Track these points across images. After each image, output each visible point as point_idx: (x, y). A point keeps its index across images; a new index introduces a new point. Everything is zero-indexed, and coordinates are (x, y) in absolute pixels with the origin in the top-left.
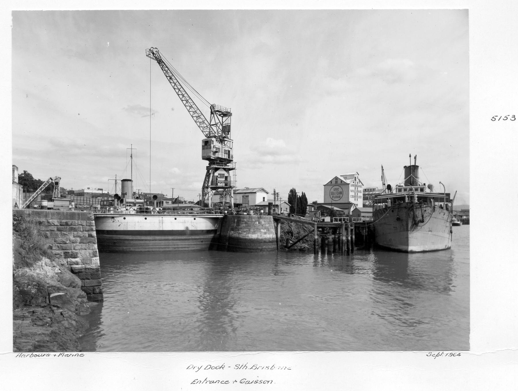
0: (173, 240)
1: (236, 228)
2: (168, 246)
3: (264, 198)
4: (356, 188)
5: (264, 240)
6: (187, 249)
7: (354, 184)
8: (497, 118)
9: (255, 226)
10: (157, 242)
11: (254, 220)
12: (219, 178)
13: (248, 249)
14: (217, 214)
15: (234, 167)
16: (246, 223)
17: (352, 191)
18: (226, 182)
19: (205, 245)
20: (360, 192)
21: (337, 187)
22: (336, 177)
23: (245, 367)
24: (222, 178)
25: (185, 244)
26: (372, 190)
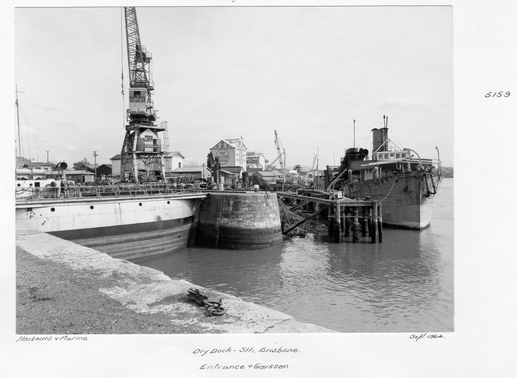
0: (139, 240)
1: (233, 213)
2: (133, 252)
3: (180, 163)
4: (241, 152)
5: (274, 229)
6: (161, 252)
7: (239, 148)
8: (492, 95)
9: (262, 210)
10: (114, 246)
11: (260, 201)
12: (146, 141)
13: (256, 244)
14: (198, 194)
15: (164, 128)
16: (249, 206)
17: (237, 155)
18: (155, 146)
19: (182, 242)
20: (244, 155)
21: (223, 151)
22: (222, 141)
23: (251, 351)
24: (150, 141)
25: (158, 244)
26: (252, 154)
